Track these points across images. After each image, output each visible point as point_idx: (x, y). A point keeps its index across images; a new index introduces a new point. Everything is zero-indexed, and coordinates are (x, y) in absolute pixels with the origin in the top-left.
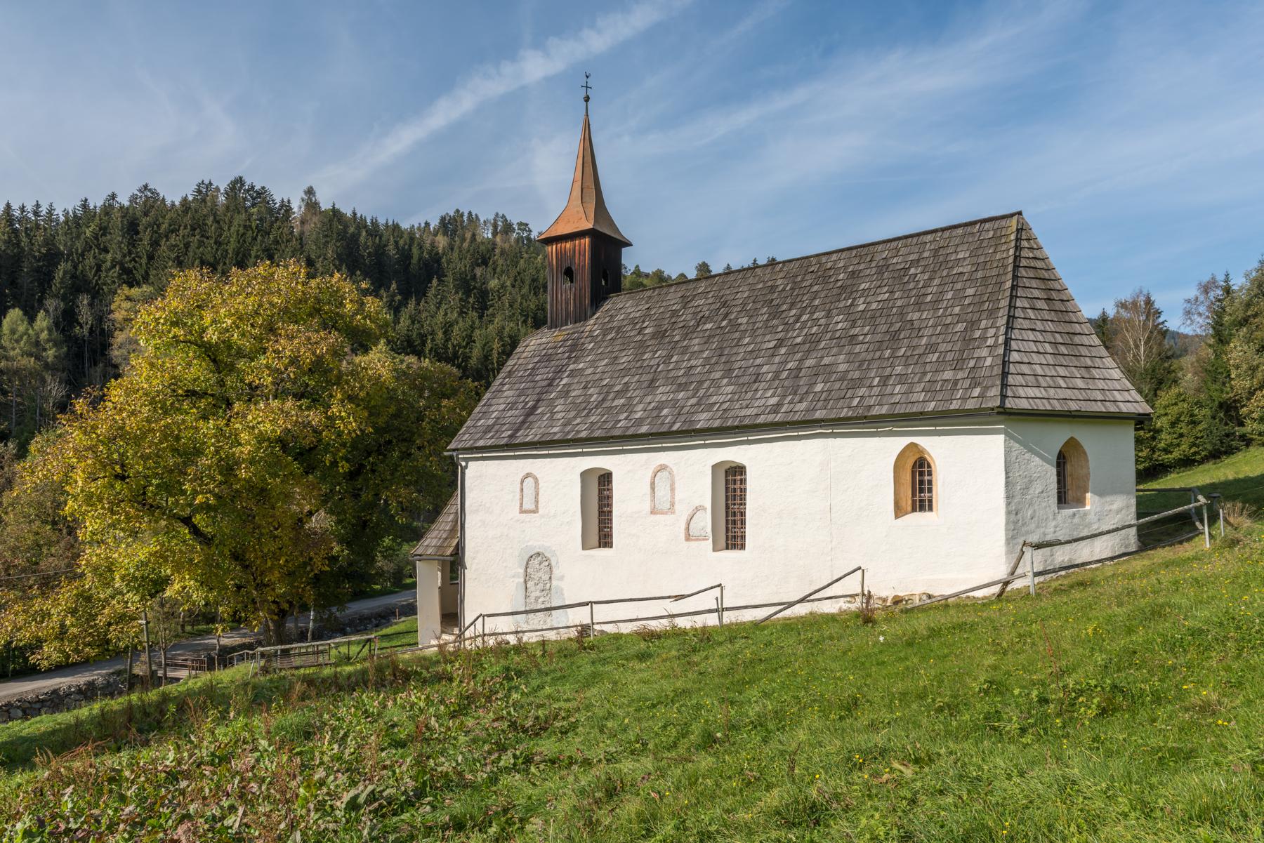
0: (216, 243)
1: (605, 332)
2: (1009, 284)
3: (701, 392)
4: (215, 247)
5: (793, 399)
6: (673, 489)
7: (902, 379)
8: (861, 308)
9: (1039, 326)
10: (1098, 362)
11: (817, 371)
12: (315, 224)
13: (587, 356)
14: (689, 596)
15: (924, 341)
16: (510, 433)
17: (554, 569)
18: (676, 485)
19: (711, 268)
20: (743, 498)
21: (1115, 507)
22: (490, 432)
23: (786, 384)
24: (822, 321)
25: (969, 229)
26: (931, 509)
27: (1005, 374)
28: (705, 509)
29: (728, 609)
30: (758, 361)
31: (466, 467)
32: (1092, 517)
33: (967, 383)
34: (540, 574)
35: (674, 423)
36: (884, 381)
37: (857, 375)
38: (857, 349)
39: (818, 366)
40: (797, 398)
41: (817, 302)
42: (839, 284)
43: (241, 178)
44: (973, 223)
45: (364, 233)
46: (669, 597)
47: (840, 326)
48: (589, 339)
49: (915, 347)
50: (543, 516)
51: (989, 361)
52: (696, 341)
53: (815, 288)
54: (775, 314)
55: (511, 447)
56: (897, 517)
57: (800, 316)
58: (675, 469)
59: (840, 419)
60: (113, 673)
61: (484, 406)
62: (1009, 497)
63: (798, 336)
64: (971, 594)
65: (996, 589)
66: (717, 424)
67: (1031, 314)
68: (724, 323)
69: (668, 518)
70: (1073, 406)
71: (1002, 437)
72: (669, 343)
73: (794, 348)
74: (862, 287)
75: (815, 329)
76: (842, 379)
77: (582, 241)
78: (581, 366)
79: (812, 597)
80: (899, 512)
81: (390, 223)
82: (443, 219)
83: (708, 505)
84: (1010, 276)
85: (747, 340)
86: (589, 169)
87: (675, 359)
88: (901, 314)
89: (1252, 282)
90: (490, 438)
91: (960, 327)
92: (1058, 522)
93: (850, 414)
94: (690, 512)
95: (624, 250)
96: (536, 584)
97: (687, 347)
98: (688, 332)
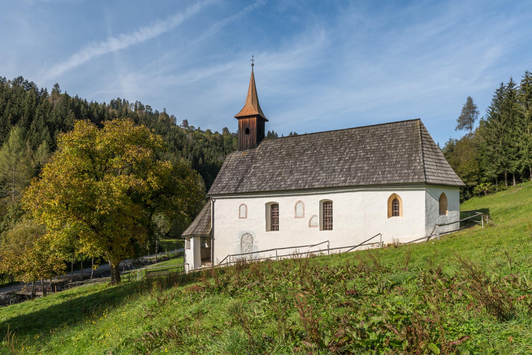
0: (19, 106)
1: (265, 153)
2: (420, 142)
3: (313, 176)
4: (18, 108)
5: (350, 178)
6: (304, 209)
7: (389, 172)
8: (369, 148)
9: (431, 156)
10: (448, 169)
11: (357, 169)
12: (60, 100)
13: (260, 161)
14: (316, 245)
15: (394, 160)
16: (234, 189)
17: (254, 239)
18: (305, 208)
19: (229, 130)
20: (332, 212)
21: (454, 215)
22: (225, 188)
23: (346, 173)
24: (354, 152)
25: (402, 123)
26: (398, 215)
27: (425, 171)
28: (317, 216)
29: (331, 249)
30: (333, 165)
31: (215, 201)
32: (448, 218)
33: (413, 174)
34: (248, 241)
35: (305, 186)
36: (383, 172)
37: (372, 170)
38: (371, 162)
39: (357, 167)
40: (352, 178)
41: (350, 146)
42: (358, 139)
43: (21, 77)
44: (404, 121)
45: (83, 106)
46: (308, 246)
47: (362, 154)
48: (258, 155)
49: (391, 162)
50: (249, 220)
51: (419, 167)
52: (306, 157)
53: (349, 141)
54: (335, 149)
55: (236, 194)
56: (388, 218)
57: (346, 150)
58: (305, 202)
59: (370, 185)
60: (7, 294)
61: (219, 179)
62: (426, 211)
63: (346, 157)
64: (414, 242)
65: (426, 239)
66: (323, 186)
67: (428, 152)
68: (315, 151)
69: (302, 219)
70: (445, 182)
71: (424, 192)
72: (294, 158)
73: (346, 161)
74: (367, 141)
75: (352, 155)
76: (368, 172)
77: (253, 119)
78: (258, 165)
79: (351, 248)
80: (388, 217)
81: (94, 102)
82: (112, 101)
83: (318, 215)
84: (420, 140)
85: (326, 158)
86: (254, 91)
87: (298, 163)
88: (384, 151)
89: (448, 146)
90: (226, 190)
91: (406, 156)
92: (440, 219)
93: (373, 183)
94: (311, 217)
95: (266, 123)
96: (246, 245)
97: (302, 160)
98: (301, 154)
